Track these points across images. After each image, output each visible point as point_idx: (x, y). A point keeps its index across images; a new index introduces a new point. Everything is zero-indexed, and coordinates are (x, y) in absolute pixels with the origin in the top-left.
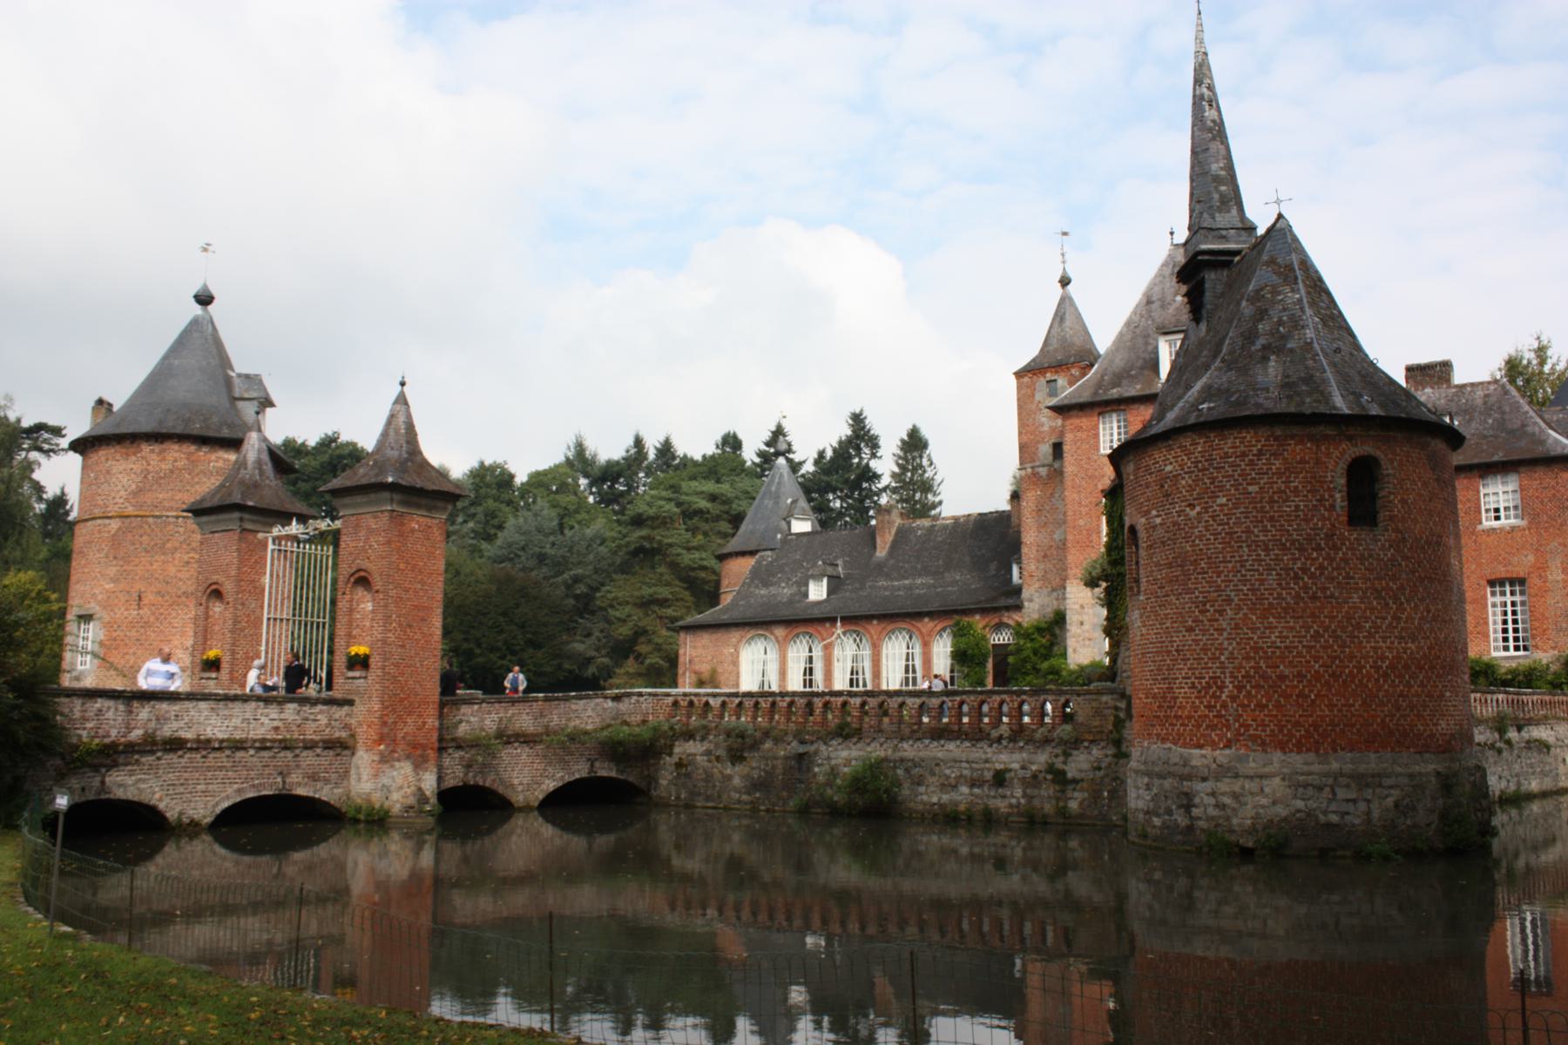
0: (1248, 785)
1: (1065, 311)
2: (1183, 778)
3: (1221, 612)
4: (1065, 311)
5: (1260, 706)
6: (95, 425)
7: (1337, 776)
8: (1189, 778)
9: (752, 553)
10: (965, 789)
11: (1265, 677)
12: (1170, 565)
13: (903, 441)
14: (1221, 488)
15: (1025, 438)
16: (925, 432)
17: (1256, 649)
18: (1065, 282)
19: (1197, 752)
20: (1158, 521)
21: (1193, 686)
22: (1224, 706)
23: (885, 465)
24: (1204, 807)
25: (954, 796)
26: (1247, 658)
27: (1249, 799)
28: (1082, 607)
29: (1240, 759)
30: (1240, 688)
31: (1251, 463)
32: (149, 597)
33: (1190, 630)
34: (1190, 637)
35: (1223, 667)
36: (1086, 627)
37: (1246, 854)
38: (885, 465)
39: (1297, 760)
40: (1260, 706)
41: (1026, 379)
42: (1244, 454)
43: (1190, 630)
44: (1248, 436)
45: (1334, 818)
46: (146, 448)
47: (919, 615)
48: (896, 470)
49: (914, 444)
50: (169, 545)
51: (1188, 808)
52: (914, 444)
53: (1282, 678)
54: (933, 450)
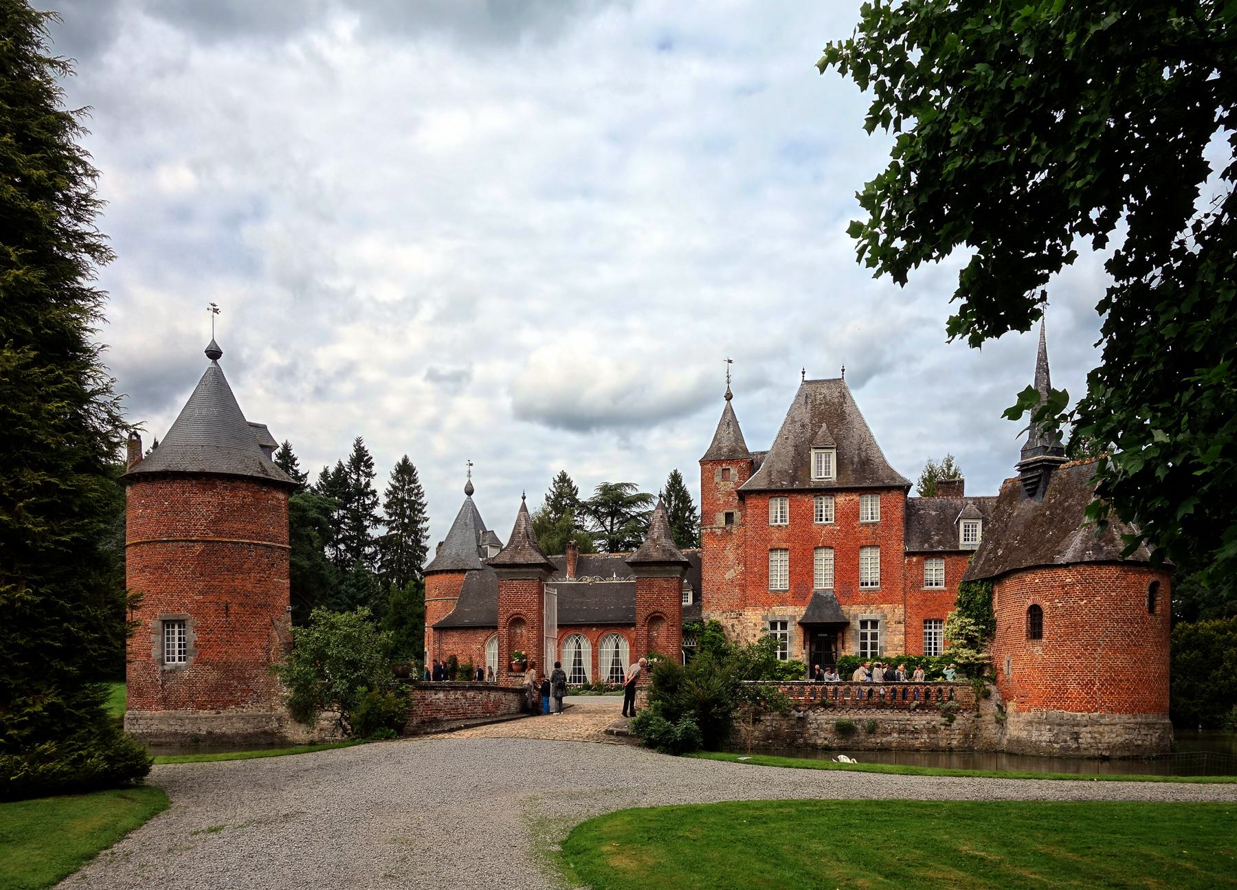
0: (1107, 728)
1: (730, 420)
2: (1073, 726)
4: (730, 420)
5: (1111, 693)
8: (1078, 725)
9: (463, 571)
10: (895, 735)
11: (1114, 680)
12: (1067, 627)
13: (399, 465)
14: (1098, 592)
15: (706, 508)
16: (413, 461)
23: (382, 483)
24: (1086, 738)
25: (889, 738)
29: (1102, 717)
32: (234, 608)
33: (1079, 658)
34: (1078, 662)
35: (1095, 675)
37: (1104, 759)
38: (382, 483)
39: (1125, 717)
40: (1111, 693)
41: (709, 466)
44: (1113, 569)
46: (220, 486)
48: (390, 488)
49: (405, 471)
50: (245, 566)
51: (1076, 739)
52: (405, 471)
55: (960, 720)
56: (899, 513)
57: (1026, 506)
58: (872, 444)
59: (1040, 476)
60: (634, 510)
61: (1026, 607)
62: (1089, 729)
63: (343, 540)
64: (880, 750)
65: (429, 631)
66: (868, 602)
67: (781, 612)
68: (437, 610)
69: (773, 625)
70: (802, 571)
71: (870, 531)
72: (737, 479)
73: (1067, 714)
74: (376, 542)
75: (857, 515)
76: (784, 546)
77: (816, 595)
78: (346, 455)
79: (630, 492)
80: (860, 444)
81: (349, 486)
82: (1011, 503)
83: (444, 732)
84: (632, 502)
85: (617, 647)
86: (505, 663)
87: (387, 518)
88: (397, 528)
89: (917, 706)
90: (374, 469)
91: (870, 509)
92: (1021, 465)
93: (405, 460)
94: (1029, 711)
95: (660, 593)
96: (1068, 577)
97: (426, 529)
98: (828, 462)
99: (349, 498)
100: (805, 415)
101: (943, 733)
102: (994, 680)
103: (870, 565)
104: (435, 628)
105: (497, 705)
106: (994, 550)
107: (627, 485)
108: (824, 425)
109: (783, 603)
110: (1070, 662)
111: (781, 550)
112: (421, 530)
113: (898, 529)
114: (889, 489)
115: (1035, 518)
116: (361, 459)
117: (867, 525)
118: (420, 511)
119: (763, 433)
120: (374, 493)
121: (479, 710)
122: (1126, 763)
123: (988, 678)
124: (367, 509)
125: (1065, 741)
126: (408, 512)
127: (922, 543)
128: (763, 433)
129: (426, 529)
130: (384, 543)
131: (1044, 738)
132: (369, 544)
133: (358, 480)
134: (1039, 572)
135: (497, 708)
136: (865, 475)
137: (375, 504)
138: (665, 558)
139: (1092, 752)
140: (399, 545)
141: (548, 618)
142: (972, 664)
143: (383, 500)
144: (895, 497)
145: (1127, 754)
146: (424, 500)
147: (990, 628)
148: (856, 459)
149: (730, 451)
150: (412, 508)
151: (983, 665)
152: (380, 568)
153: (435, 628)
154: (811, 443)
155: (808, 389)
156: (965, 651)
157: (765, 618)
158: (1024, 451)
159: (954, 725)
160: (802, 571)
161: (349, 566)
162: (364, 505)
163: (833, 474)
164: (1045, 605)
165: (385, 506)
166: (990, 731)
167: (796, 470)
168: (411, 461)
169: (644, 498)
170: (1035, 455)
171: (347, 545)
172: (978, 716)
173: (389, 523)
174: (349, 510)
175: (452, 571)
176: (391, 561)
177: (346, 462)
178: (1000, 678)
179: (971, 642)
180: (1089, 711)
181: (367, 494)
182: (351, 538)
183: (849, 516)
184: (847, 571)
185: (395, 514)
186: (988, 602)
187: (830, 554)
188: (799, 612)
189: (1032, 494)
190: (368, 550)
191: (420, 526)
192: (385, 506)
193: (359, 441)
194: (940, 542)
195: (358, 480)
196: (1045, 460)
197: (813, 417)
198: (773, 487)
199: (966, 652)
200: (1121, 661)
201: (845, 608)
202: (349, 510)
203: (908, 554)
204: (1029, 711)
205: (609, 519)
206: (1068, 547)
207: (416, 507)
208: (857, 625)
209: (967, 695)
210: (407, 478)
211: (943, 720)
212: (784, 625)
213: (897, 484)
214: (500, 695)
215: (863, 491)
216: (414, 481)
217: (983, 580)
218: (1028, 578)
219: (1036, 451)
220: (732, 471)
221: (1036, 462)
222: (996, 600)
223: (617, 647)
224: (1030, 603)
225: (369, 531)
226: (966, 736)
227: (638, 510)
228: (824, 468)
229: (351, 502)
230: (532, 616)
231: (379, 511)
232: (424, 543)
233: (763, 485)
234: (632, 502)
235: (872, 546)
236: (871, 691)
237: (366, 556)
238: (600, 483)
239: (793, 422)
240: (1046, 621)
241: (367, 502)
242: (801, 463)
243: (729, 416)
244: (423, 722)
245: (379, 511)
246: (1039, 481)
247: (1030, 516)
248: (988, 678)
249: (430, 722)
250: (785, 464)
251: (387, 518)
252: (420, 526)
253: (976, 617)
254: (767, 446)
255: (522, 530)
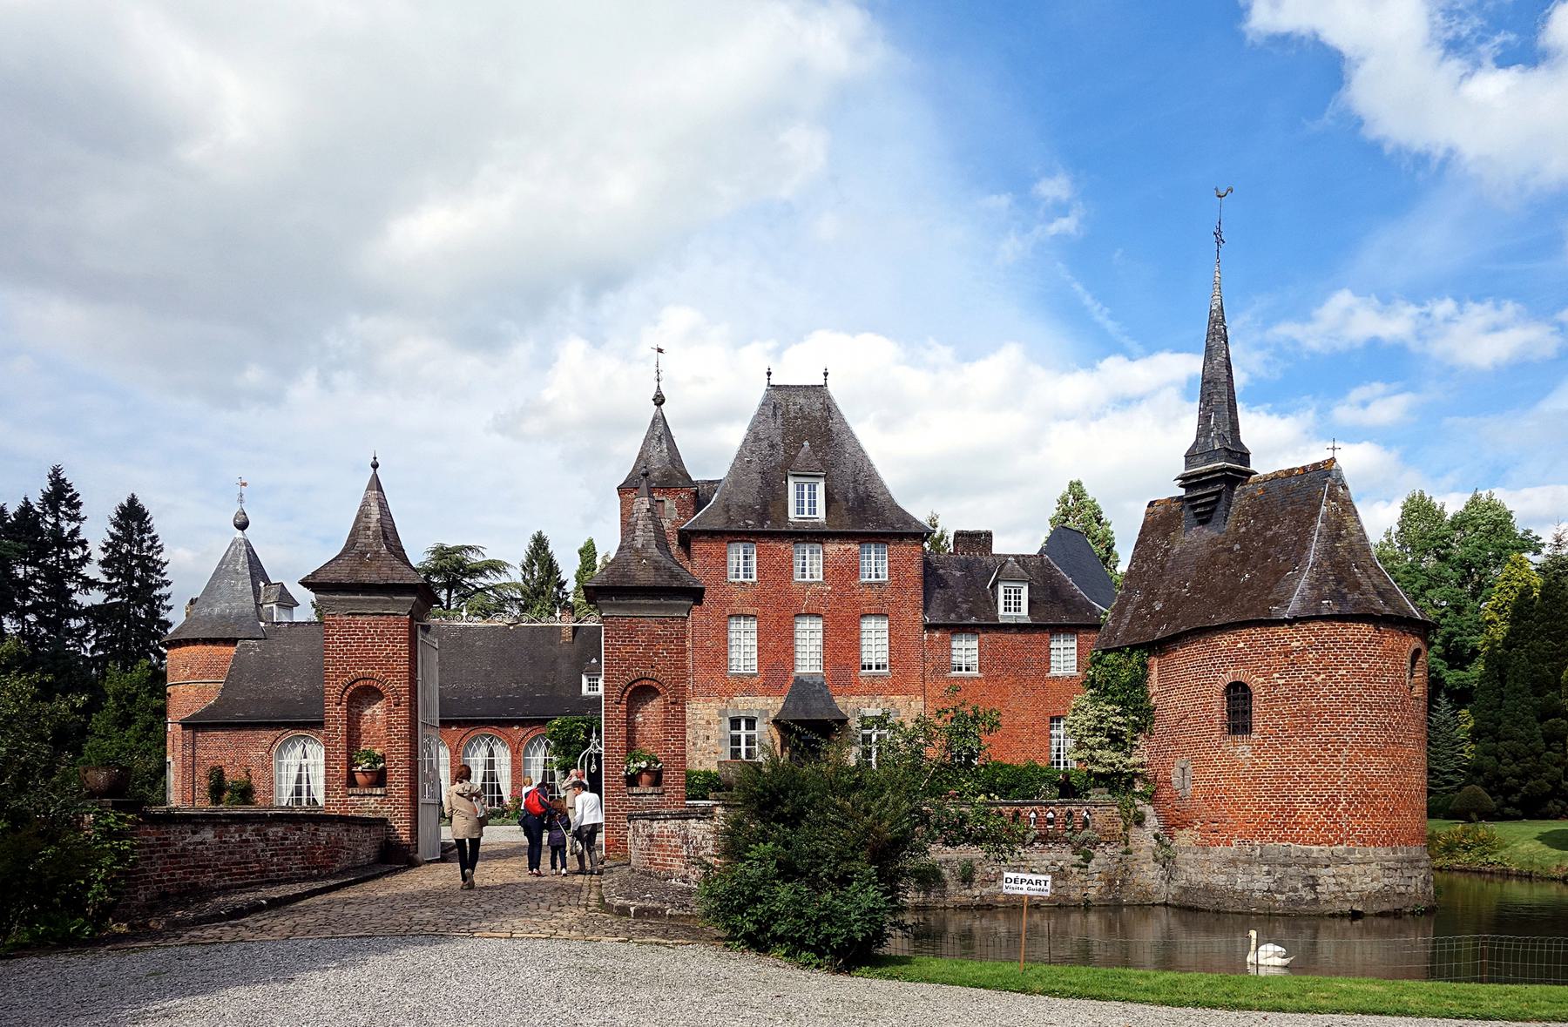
0: (1357, 869)
1: (660, 431)
2: (1308, 866)
3: (1339, 751)
4: (660, 431)
6: (1304, 609)
7: (1402, 861)
8: (1315, 865)
9: (231, 642)
11: (1367, 796)
13: (122, 507)
17: (1362, 777)
18: (659, 400)
19: (1315, 848)
20: (1281, 682)
21: (1314, 801)
22: (1339, 816)
23: (96, 531)
24: (1328, 881)
26: (1356, 783)
27: (1358, 879)
28: (708, 723)
30: (1350, 804)
31: (1365, 647)
33: (1314, 762)
34: (1312, 768)
36: (712, 741)
38: (96, 531)
39: (1382, 852)
42: (1359, 641)
43: (1314, 762)
44: (1364, 627)
45: (1403, 889)
47: (509, 723)
49: (132, 516)
51: (1313, 887)
52: (132, 516)
53: (1376, 797)
54: (158, 525)
55: (1100, 857)
56: (916, 570)
57: (1193, 538)
58: (872, 476)
59: (1218, 493)
60: (481, 581)
61: (1221, 686)
62: (1332, 870)
63: (31, 610)
64: (978, 908)
65: (173, 729)
66: (873, 691)
67: (745, 704)
68: (191, 682)
69: (735, 723)
70: (777, 648)
71: (874, 593)
72: (675, 516)
73: (1296, 848)
74: (89, 612)
75: (856, 572)
76: (750, 611)
77: (799, 681)
78: (36, 490)
79: (474, 558)
80: (855, 474)
81: (42, 532)
82: (1166, 535)
83: (216, 918)
84: (477, 571)
85: (491, 754)
86: (342, 771)
87: (104, 579)
88: (121, 594)
89: (1036, 838)
90: (83, 512)
91: (875, 565)
92: (1184, 478)
93: (132, 501)
94: (1228, 844)
95: (649, 646)
96: (1295, 639)
97: (167, 597)
98: (813, 496)
99: (43, 550)
100: (774, 429)
101: (1076, 878)
102: (1151, 798)
103: (875, 641)
104: (185, 725)
105: (333, 850)
106: (1147, 602)
107: (470, 548)
108: (806, 443)
109: (750, 691)
110: (1300, 770)
111: (746, 617)
112: (160, 598)
113: (915, 594)
114: (901, 537)
115: (1213, 554)
116: (60, 494)
117: (870, 585)
118: (154, 569)
119: (713, 450)
120: (83, 544)
121: (295, 864)
122: (1385, 922)
123: (1141, 795)
124: (72, 568)
125: (1295, 890)
126: (138, 572)
127: (947, 612)
128: (713, 450)
129: (167, 597)
130: (96, 614)
131: (1257, 886)
132: (76, 616)
133: (56, 525)
134: (1245, 631)
135: (334, 857)
136: (866, 516)
137: (85, 559)
138: (662, 581)
139: (1338, 907)
140: (125, 617)
141: (424, 690)
142: (1120, 774)
143: (98, 555)
144: (906, 549)
145: (1386, 907)
146: (163, 557)
147: (1143, 717)
148: (851, 495)
149: (664, 475)
150: (145, 569)
151: (1136, 775)
152: (93, 650)
153: (185, 725)
154: (787, 467)
155: (778, 396)
156: (1106, 753)
157: (722, 713)
158: (1190, 457)
159: (1092, 865)
160: (777, 648)
161: (42, 644)
162: (67, 561)
163: (821, 514)
164: (1256, 682)
165: (103, 563)
166: (1149, 875)
167: (765, 505)
168: (142, 501)
169: (495, 567)
170: (1208, 461)
171: (38, 615)
172: (1127, 852)
173: (107, 587)
174: (43, 566)
175: (206, 641)
176: (111, 641)
177: (36, 500)
178: (1165, 793)
179: (1116, 739)
180: (1330, 843)
181: (71, 546)
182: (48, 607)
183: (842, 574)
184: (843, 646)
185: (119, 575)
186: (1139, 681)
187: (818, 625)
188: (774, 704)
189: (1204, 520)
190: (74, 623)
191: (157, 593)
192: (103, 563)
193: (56, 472)
194: (971, 612)
195: (56, 525)
196: (1229, 469)
197: (784, 435)
198: (734, 528)
199: (1108, 755)
200: (1377, 767)
201: (839, 701)
202: (43, 566)
203: (929, 627)
204: (1228, 844)
205: (445, 591)
206: (1290, 593)
207: (151, 566)
208: (854, 723)
209: (1111, 821)
210: (135, 525)
211: (1076, 859)
212: (751, 723)
213: (913, 530)
214: (337, 831)
215: (865, 538)
216: (149, 530)
217: (1134, 648)
218: (1224, 641)
219: (1212, 455)
220: (667, 504)
221: (1213, 471)
222: (1154, 675)
223: (491, 754)
224: (1228, 679)
225: (75, 597)
226: (1111, 882)
227: (486, 582)
228: (806, 502)
229: (46, 556)
230: (400, 683)
231: (92, 571)
232: (165, 616)
233: (718, 524)
234: (477, 571)
235: (880, 615)
236: (1017, 813)
237: (70, 632)
238: (432, 545)
239: (757, 439)
240: (1258, 706)
241: (72, 556)
242: (773, 498)
243: (660, 429)
244: (164, 896)
245: (92, 571)
246: (1217, 501)
247: (1205, 552)
248: (1141, 795)
249: (181, 895)
250: (749, 495)
251: (104, 579)
252: (157, 593)
253: (1122, 703)
254: (720, 472)
255: (373, 525)
